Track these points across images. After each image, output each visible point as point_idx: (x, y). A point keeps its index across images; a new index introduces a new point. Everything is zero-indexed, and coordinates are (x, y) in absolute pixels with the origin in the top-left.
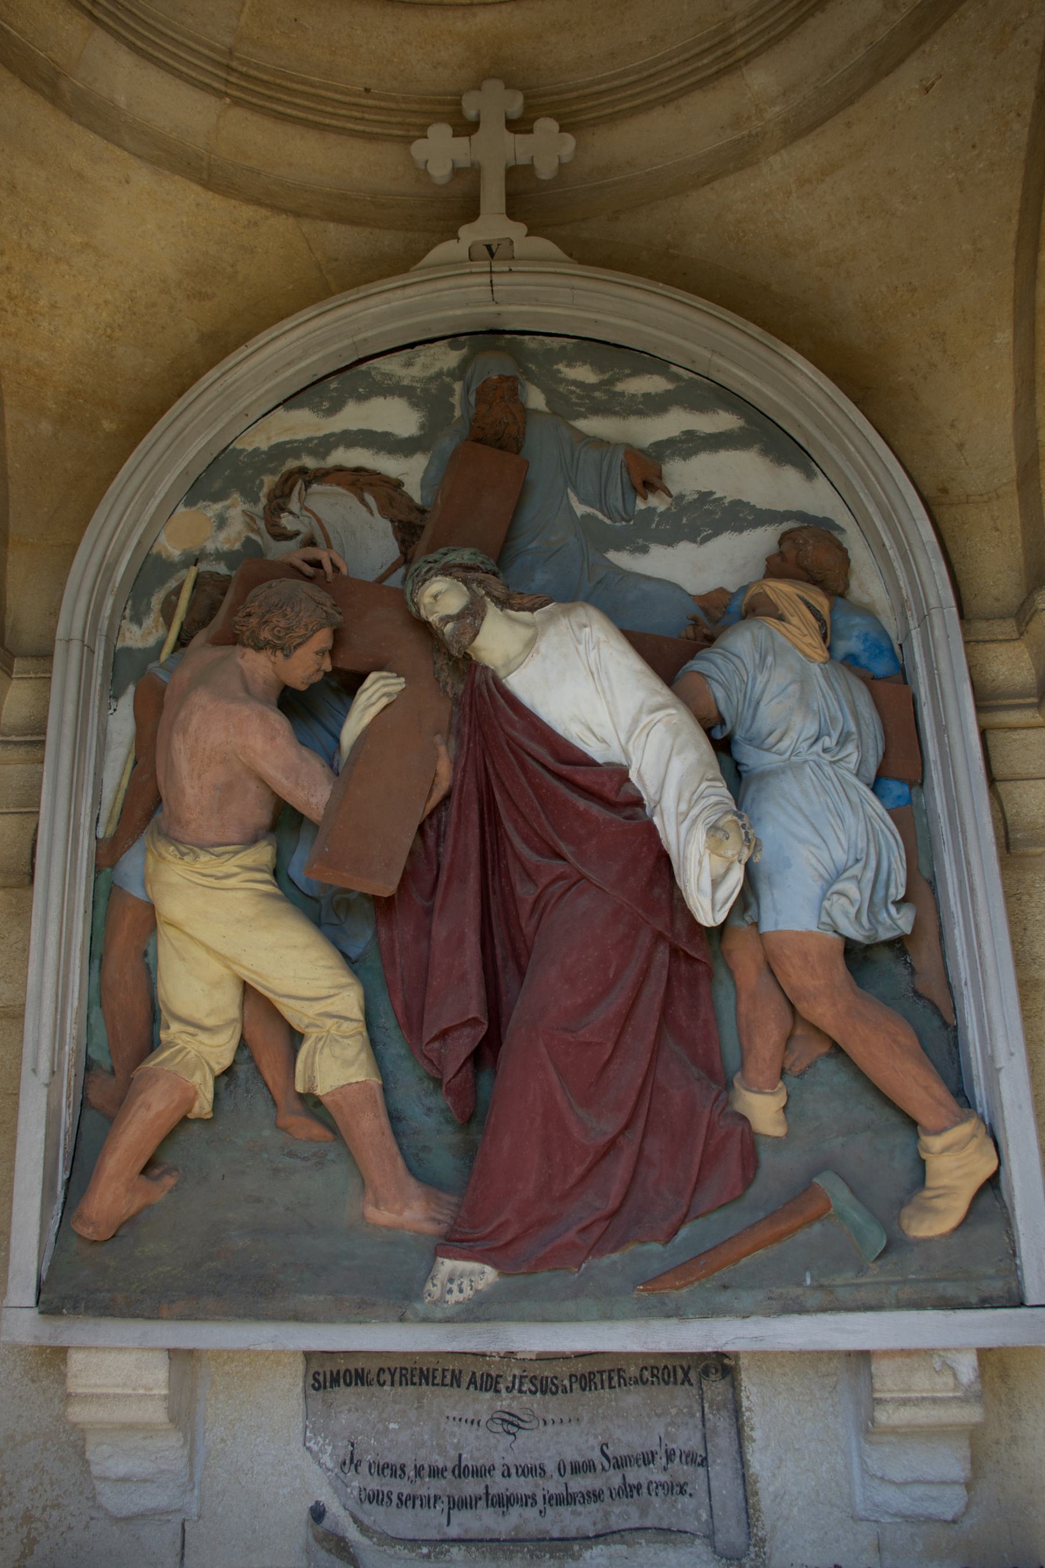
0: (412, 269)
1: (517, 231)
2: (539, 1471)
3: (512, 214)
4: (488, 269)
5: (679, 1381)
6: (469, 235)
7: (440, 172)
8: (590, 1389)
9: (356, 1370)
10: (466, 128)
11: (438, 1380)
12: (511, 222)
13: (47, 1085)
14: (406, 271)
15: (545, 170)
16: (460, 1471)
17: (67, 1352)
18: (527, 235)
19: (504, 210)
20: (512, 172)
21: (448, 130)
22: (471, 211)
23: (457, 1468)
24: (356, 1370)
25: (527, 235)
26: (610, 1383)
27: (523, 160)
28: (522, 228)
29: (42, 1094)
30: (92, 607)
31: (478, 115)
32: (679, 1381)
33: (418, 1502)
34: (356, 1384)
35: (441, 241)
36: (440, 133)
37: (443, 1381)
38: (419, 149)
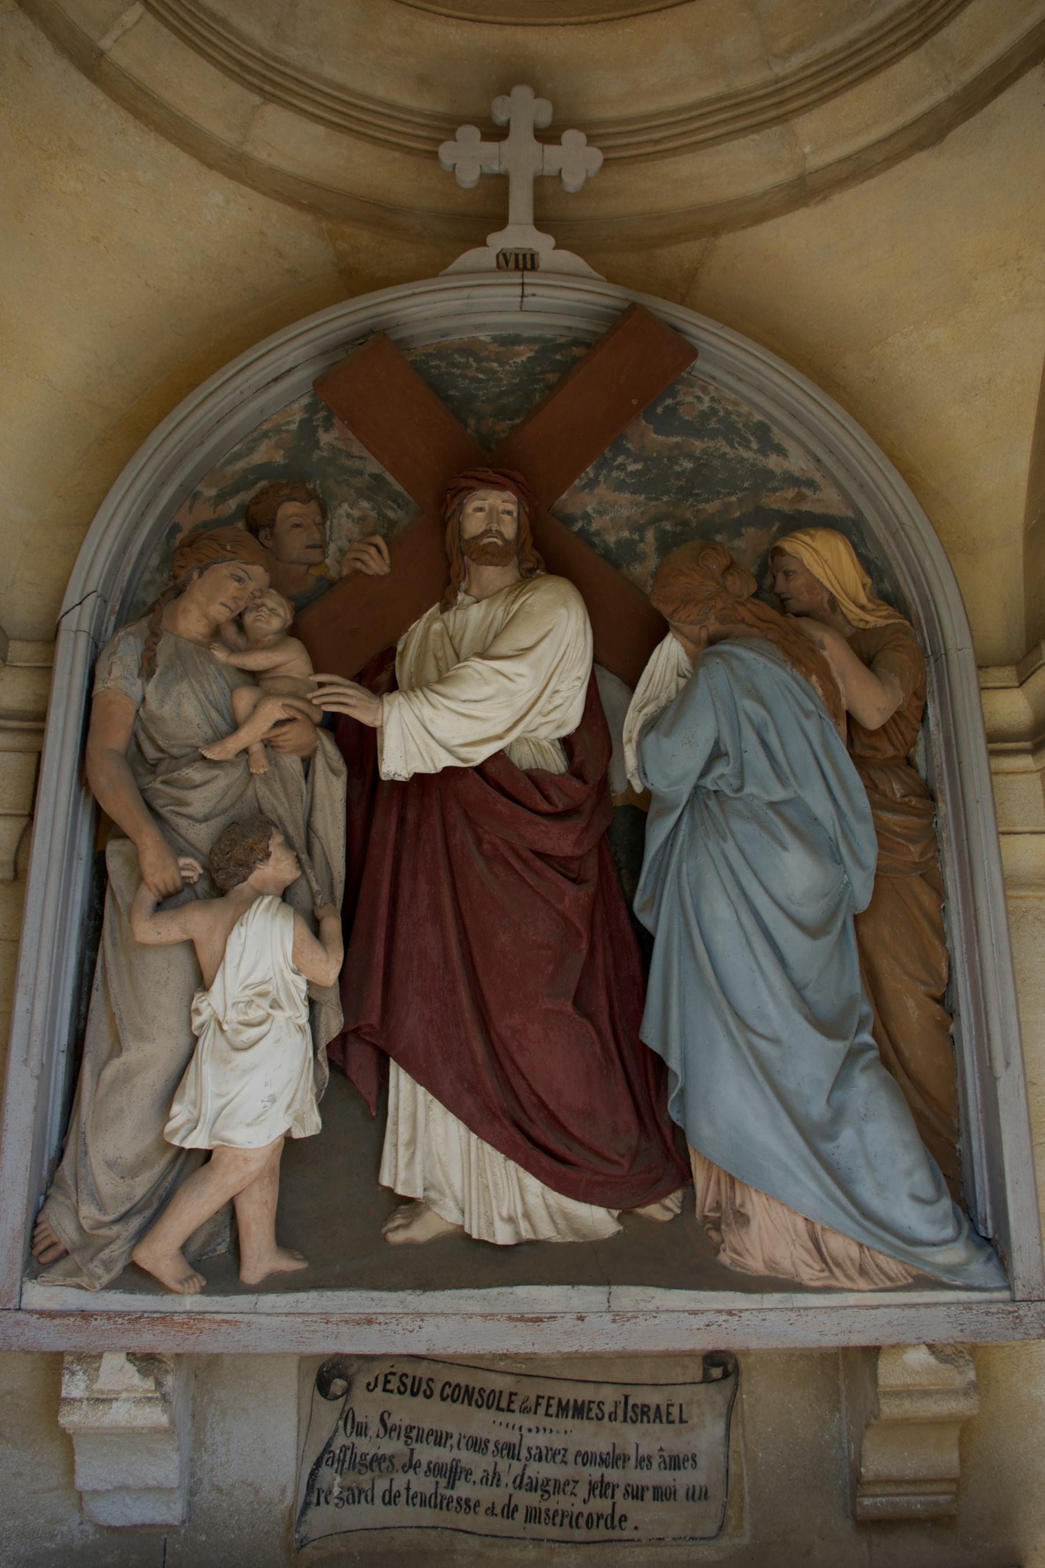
0: (441, 273)
1: (542, 244)
2: (455, 1504)
3: (541, 223)
4: (520, 281)
5: (652, 1419)
6: (499, 241)
7: (468, 178)
8: (642, 1422)
9: (467, 1387)
10: (496, 133)
11: (504, 1404)
12: (540, 234)
13: (37, 1077)
14: (435, 275)
15: (573, 182)
16: (390, 1496)
17: (878, 1354)
18: (554, 249)
19: (531, 220)
20: (539, 181)
21: (475, 132)
22: (501, 222)
23: (387, 1493)
24: (467, 1387)
25: (554, 249)
26: (588, 1414)
27: (550, 170)
28: (549, 241)
29: (32, 1085)
30: (947, 688)
31: (509, 122)
32: (652, 1419)
33: (566, 1521)
34: (462, 1402)
35: (464, 251)
36: (470, 133)
37: (509, 1406)
38: (447, 152)
